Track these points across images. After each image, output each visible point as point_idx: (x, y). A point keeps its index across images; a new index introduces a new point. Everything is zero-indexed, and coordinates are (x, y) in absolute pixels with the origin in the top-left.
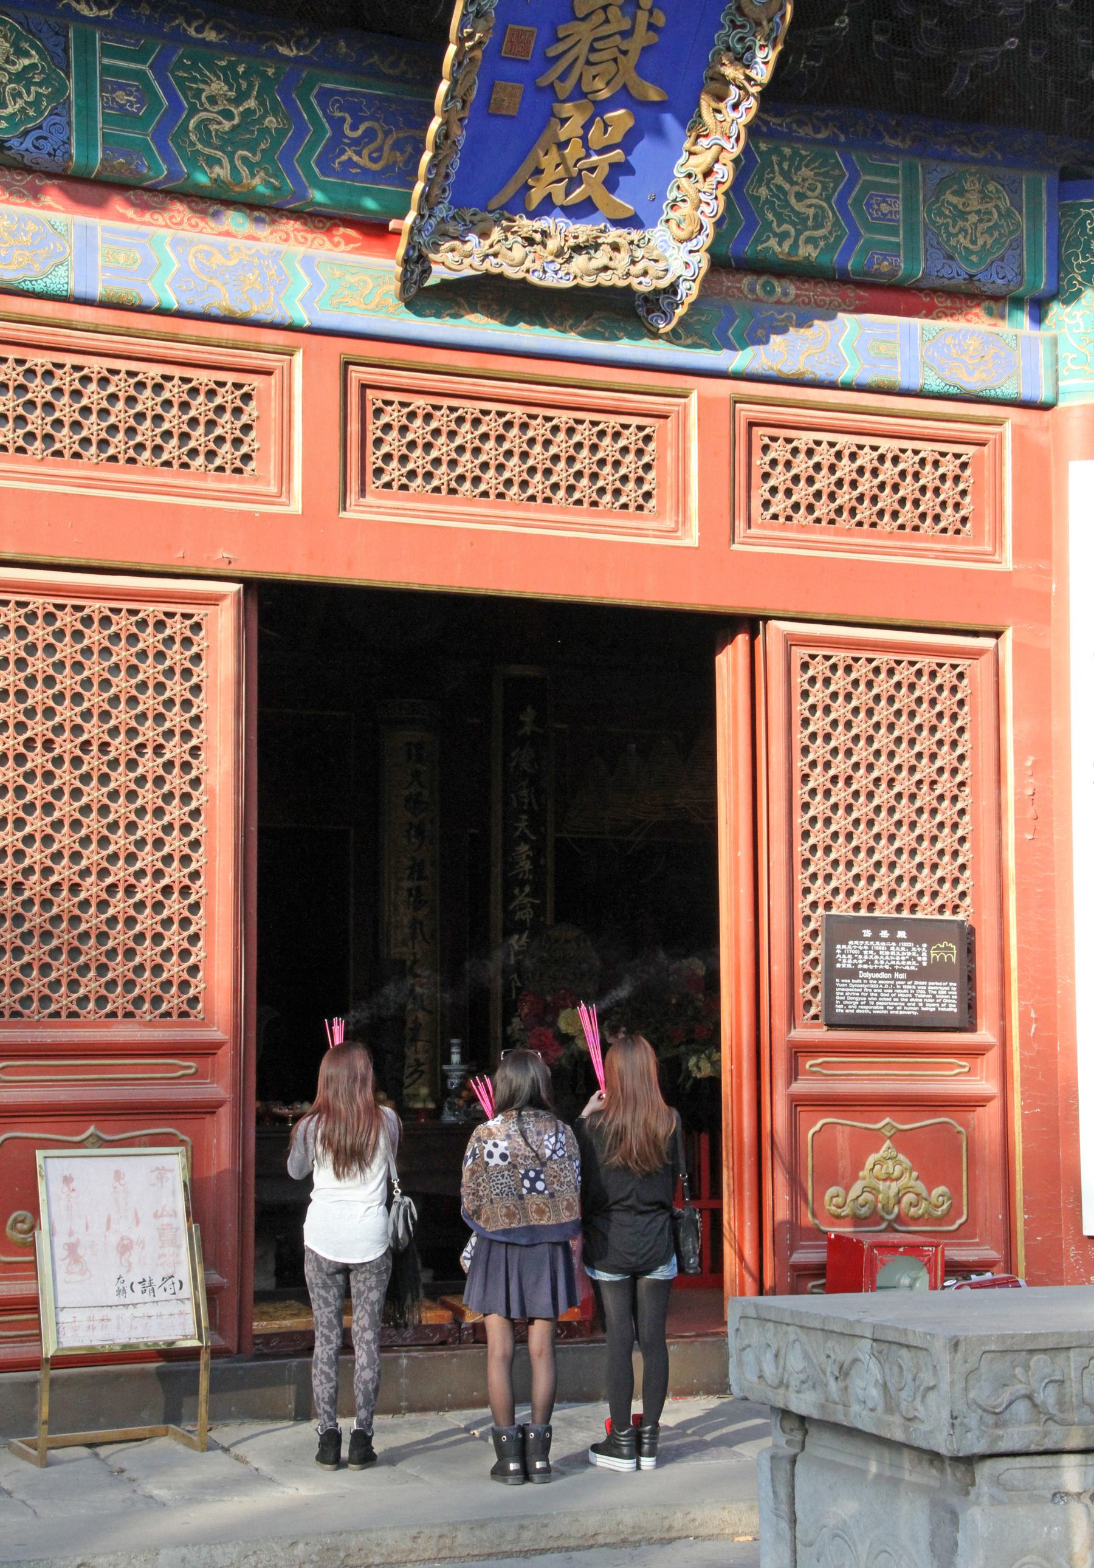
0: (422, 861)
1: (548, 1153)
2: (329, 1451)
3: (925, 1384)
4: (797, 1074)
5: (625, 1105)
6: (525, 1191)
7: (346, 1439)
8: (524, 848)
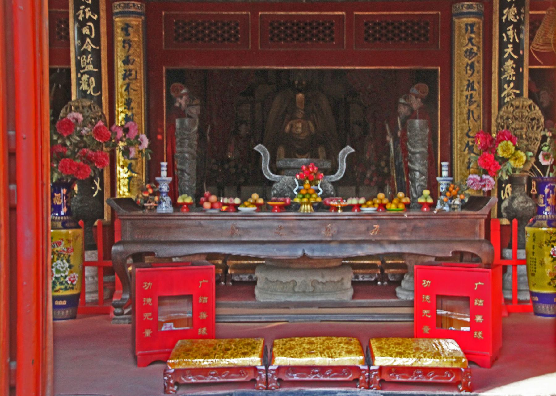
0: (473, 82)
8: (510, 63)
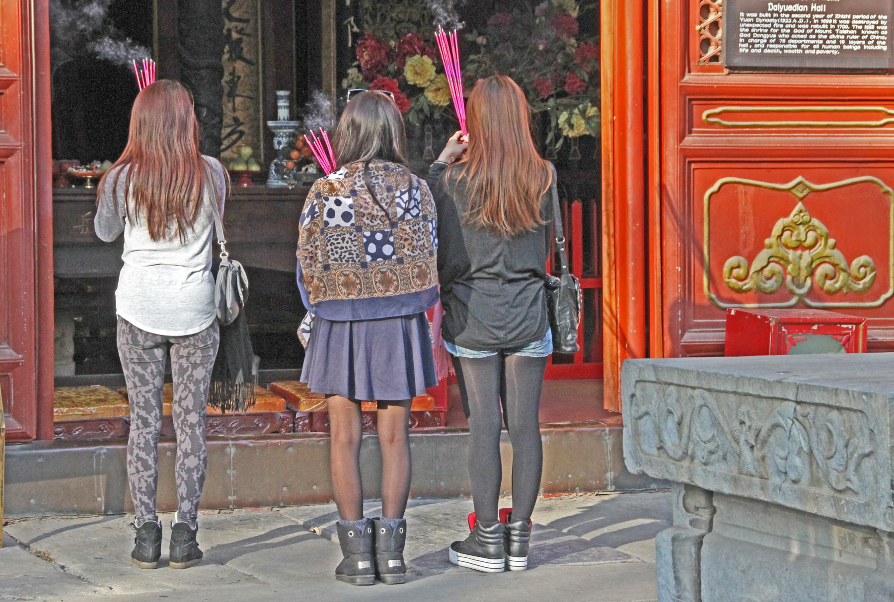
1: (400, 212)
2: (148, 547)
3: (860, 451)
4: (691, 126)
5: (490, 163)
6: (368, 258)
7: (167, 534)
